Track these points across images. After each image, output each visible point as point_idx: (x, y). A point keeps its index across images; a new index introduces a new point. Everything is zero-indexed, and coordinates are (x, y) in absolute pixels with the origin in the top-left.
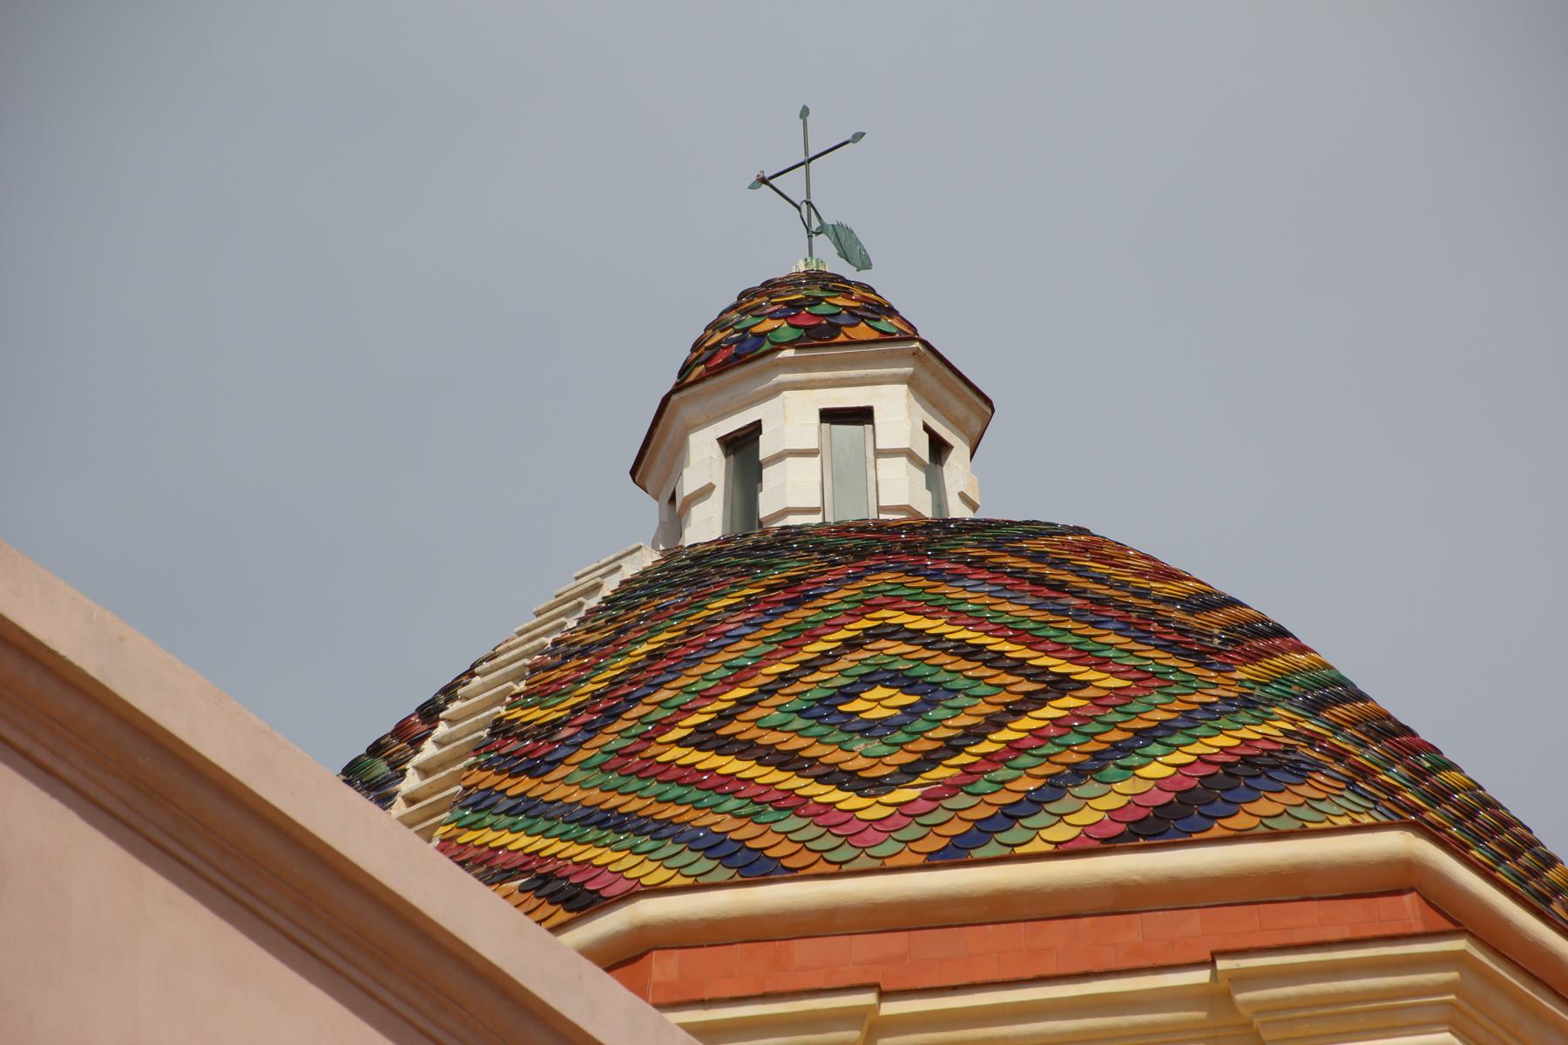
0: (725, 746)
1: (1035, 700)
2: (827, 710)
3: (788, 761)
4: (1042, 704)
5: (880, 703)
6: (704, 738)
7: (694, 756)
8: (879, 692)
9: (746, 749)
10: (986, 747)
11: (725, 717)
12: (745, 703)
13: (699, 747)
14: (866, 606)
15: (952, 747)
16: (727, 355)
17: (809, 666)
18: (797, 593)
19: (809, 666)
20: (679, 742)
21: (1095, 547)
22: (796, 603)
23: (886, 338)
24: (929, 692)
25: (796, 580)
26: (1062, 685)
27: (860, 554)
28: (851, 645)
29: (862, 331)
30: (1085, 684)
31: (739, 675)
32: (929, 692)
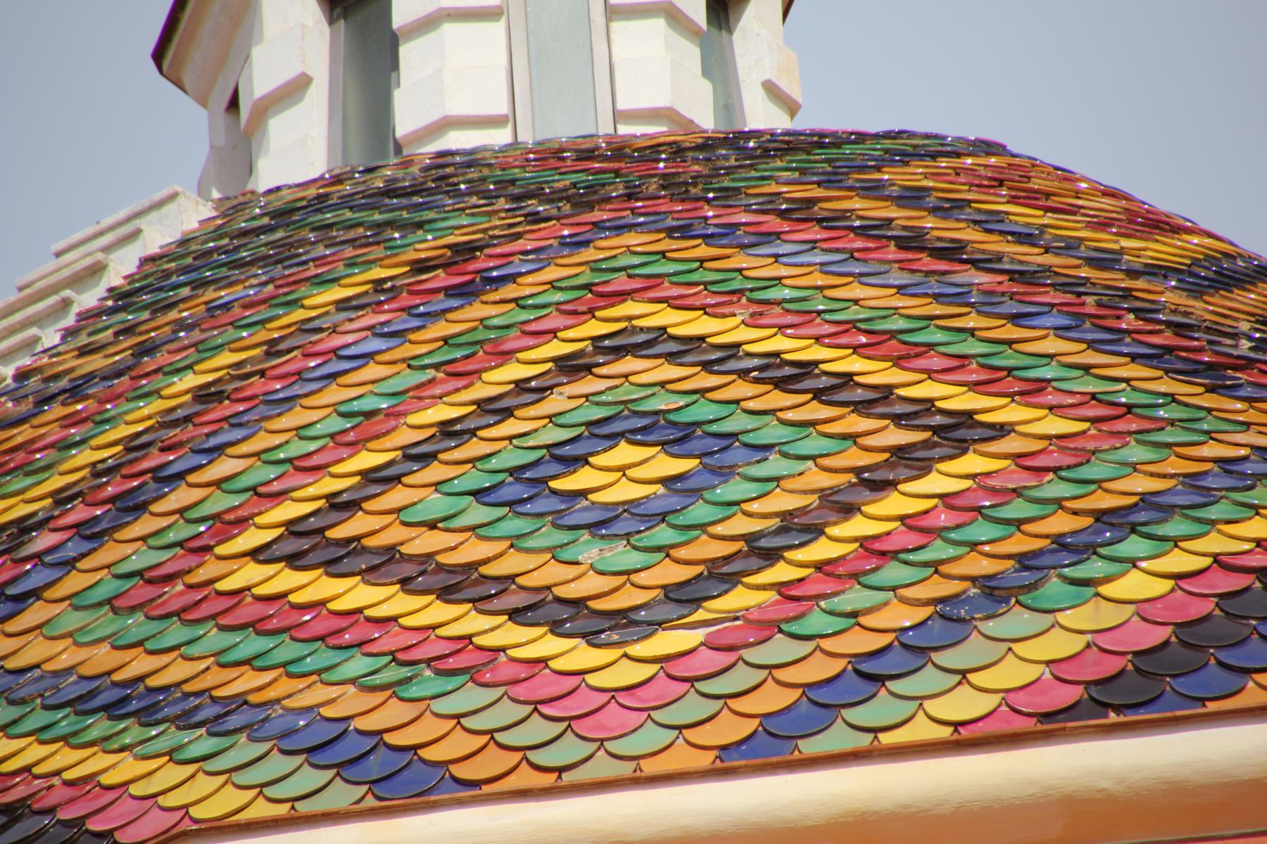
0: (342, 558)
1: (909, 461)
3: (458, 584)
4: (924, 468)
7: (284, 579)
8: (624, 453)
9: (383, 564)
10: (821, 550)
12: (379, 479)
13: (294, 561)
20: (255, 554)
21: (1018, 178)
25: (466, 251)
26: (959, 432)
27: (585, 199)
28: (572, 367)
30: (1002, 430)
31: (364, 426)
32: (712, 450)
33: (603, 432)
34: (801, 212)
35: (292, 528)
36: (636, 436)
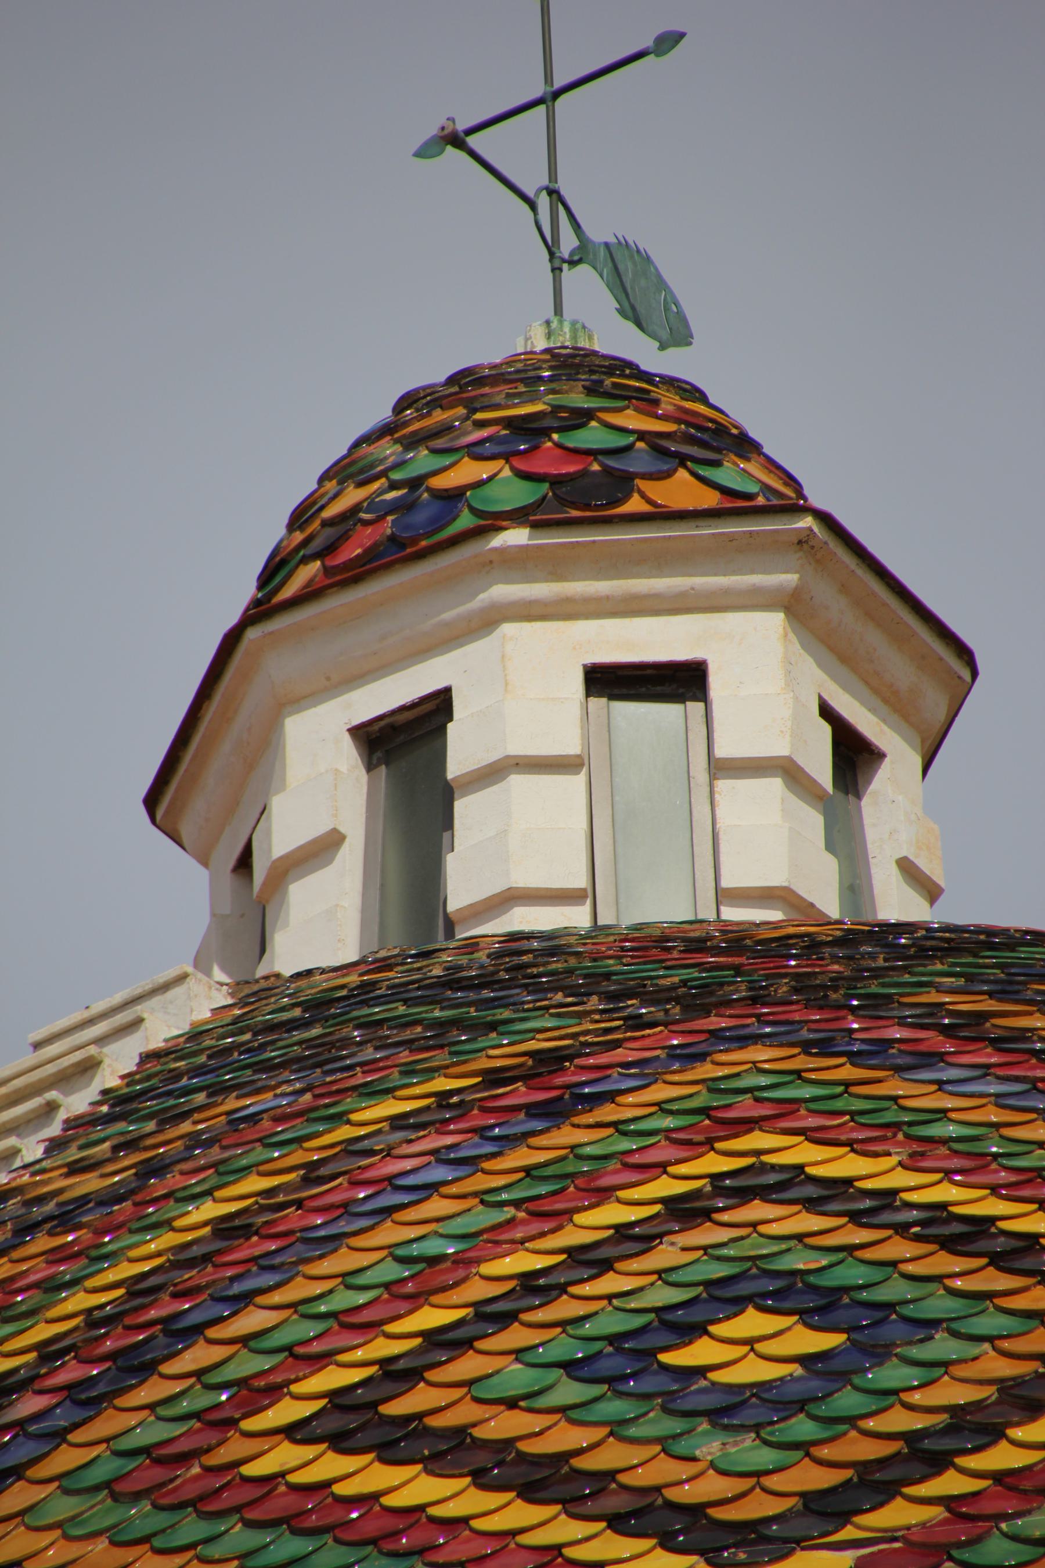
2: (630, 1362)
5: (753, 1348)
6: (351, 1422)
7: (329, 1465)
8: (753, 1322)
9: (449, 1450)
10: (1002, 1457)
11: (398, 1375)
12: (444, 1342)
13: (340, 1442)
14: (717, 1124)
15: (925, 1455)
16: (366, 537)
17: (590, 1260)
18: (555, 1089)
19: (590, 1260)
20: (294, 1432)
22: (553, 1112)
23: (736, 505)
24: (869, 1327)
25: (551, 1061)
28: (684, 1211)
29: (681, 490)
32: (869, 1327)
33: (725, 1296)
34: (969, 1029)
35: (338, 1400)
36: (761, 1302)
